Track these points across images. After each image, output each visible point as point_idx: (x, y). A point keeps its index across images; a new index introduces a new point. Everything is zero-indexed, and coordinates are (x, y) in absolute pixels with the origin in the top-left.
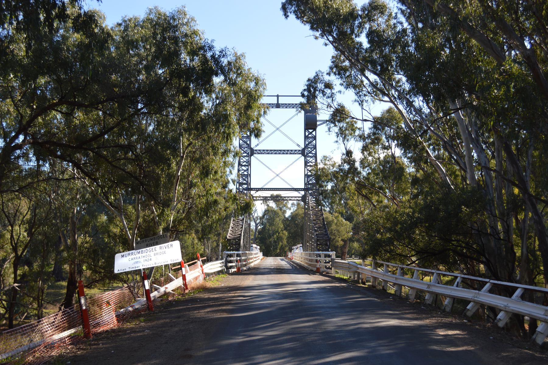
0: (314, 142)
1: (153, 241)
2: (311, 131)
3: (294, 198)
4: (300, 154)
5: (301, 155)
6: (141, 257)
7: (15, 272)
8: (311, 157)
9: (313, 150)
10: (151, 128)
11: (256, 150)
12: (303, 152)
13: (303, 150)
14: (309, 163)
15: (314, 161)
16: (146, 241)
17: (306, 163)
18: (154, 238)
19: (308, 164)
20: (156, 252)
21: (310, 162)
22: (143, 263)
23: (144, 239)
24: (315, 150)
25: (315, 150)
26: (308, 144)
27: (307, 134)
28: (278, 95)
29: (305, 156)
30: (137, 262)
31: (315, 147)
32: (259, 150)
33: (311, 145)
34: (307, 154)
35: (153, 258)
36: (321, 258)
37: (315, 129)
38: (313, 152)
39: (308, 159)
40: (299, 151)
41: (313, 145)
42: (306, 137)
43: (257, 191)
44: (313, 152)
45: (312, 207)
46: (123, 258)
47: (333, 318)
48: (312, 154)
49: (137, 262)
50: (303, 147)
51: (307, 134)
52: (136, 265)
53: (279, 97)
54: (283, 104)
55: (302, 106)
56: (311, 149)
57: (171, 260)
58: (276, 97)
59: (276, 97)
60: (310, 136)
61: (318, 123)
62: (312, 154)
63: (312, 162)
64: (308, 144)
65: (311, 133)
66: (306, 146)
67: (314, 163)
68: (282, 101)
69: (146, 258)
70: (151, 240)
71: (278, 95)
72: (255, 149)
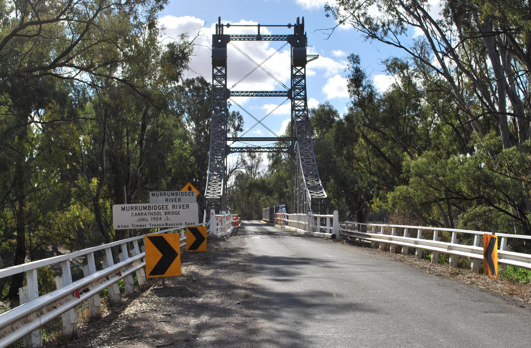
0: (303, 81)
2: (299, 68)
3: (263, 150)
4: (285, 96)
5: (287, 98)
6: (147, 214)
8: (300, 100)
9: (302, 92)
10: (108, 73)
11: (233, 92)
12: (289, 94)
14: (297, 107)
15: (303, 104)
16: (165, 194)
17: (293, 107)
18: (177, 194)
19: (296, 109)
20: (167, 211)
21: (298, 106)
22: (150, 222)
24: (304, 92)
25: (304, 92)
26: (296, 85)
27: (303, 71)
29: (293, 99)
31: (304, 88)
32: (237, 92)
33: (300, 85)
34: (295, 96)
35: (164, 217)
36: (327, 227)
37: (304, 67)
38: (302, 94)
39: (296, 102)
40: (285, 92)
41: (302, 86)
42: (293, 76)
43: (235, 141)
44: (302, 94)
47: (266, 299)
48: (301, 96)
49: (143, 220)
50: (290, 88)
51: (294, 72)
52: (142, 223)
53: (261, 28)
54: (265, 36)
55: (290, 39)
56: (300, 90)
59: (257, 27)
60: (298, 74)
61: (308, 59)
62: (301, 96)
63: (300, 106)
64: (296, 85)
65: (299, 71)
66: (293, 87)
67: (303, 108)
68: (265, 31)
69: (153, 216)
70: (173, 194)
72: (231, 90)
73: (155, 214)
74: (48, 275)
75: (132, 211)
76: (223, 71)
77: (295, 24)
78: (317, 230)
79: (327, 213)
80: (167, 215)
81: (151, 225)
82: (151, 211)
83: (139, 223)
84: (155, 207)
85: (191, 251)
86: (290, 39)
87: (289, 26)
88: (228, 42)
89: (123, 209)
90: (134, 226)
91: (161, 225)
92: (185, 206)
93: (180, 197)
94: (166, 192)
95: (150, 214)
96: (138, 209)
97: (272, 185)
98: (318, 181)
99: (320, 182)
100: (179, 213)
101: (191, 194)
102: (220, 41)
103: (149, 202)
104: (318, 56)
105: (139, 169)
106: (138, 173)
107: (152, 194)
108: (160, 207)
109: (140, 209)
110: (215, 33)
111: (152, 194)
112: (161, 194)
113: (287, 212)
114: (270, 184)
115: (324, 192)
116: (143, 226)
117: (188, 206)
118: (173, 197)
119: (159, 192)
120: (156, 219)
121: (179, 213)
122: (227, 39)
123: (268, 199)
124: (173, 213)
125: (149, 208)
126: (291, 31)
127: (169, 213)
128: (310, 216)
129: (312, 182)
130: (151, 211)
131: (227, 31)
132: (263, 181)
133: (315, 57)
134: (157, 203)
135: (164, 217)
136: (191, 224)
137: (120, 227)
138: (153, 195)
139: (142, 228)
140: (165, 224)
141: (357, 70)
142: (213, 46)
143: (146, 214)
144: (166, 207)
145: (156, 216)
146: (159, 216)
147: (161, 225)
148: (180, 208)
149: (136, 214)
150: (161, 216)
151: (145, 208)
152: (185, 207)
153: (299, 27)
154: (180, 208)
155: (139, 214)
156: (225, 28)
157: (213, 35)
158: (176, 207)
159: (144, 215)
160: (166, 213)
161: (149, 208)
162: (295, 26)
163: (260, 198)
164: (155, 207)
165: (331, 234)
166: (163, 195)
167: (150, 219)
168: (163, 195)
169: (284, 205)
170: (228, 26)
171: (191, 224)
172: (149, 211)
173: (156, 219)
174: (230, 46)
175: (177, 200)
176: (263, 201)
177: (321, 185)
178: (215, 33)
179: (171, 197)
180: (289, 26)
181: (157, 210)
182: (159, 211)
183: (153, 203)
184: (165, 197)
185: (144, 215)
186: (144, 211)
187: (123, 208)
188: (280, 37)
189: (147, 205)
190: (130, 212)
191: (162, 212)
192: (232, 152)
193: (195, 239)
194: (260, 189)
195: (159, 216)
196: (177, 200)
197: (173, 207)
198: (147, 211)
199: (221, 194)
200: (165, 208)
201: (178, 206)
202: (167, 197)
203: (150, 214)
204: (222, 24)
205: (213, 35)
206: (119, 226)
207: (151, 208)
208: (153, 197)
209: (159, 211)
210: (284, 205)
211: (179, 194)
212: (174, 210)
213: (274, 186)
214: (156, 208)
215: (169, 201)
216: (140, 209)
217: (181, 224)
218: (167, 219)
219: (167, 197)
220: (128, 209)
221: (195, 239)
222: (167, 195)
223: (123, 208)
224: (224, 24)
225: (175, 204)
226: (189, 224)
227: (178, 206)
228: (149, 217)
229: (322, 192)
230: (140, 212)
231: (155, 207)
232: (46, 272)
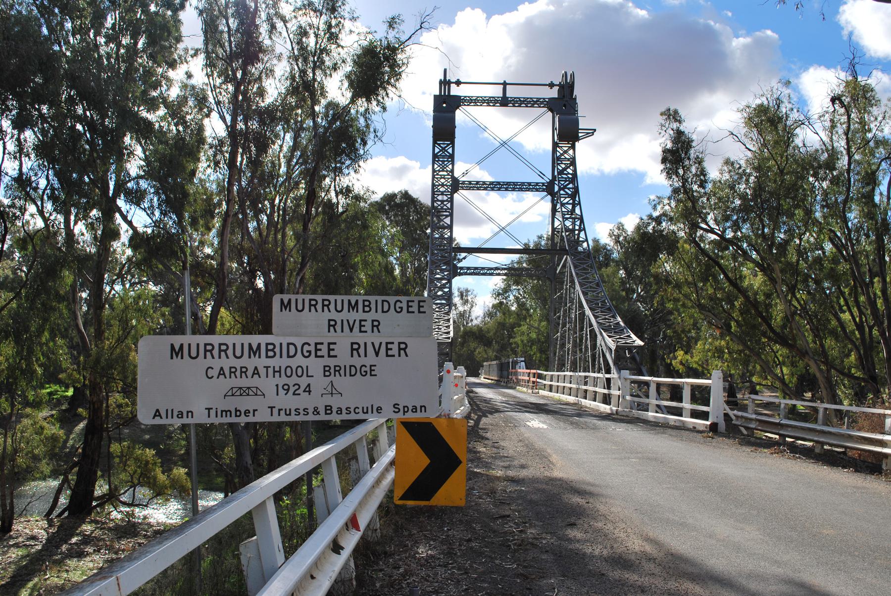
1: (360, 315)
5: (546, 193)
6: (262, 371)
7: (297, 65)
12: (549, 188)
13: (551, 184)
16: (326, 305)
20: (332, 362)
22: (272, 398)
23: (319, 298)
28: (505, 82)
30: (244, 391)
45: (560, 297)
46: (177, 360)
49: (244, 391)
52: (245, 403)
57: (395, 406)
58: (502, 86)
59: (502, 86)
68: (511, 92)
69: (284, 380)
70: (353, 307)
71: (505, 82)
73: (289, 371)
74: (151, 466)
75: (209, 361)
76: (450, 151)
77: (560, 83)
78: (650, 408)
79: (644, 370)
80: (332, 378)
81: (275, 411)
82: (275, 362)
83: (232, 404)
84: (292, 348)
85: (410, 503)
86: (551, 105)
87: (551, 85)
88: (458, 108)
89: (176, 352)
90: (213, 412)
91: (311, 411)
92: (395, 347)
93: (379, 316)
94: (332, 298)
95: (271, 371)
96: (230, 352)
97: (491, 334)
98: (614, 317)
99: (619, 319)
100: (371, 371)
101: (415, 308)
102: (444, 105)
103: (267, 330)
104: (595, 130)
105: (299, 278)
106: (297, 286)
107: (282, 300)
108: (306, 348)
109: (238, 354)
110: (438, 93)
111: (282, 300)
112: (313, 305)
113: (527, 368)
114: (489, 332)
115: (633, 335)
116: (247, 412)
117: (403, 348)
118: (354, 316)
119: (307, 297)
120: (292, 390)
121: (371, 371)
122: (457, 102)
123: (485, 351)
124: (352, 371)
125: (271, 350)
126: (554, 93)
127: (337, 370)
128: (626, 379)
129: (605, 319)
130: (275, 362)
131: (455, 91)
132: (480, 329)
133: (588, 133)
134: (297, 335)
135: (319, 382)
136: (415, 410)
137: (163, 415)
138: (285, 306)
139: (243, 420)
140: (322, 410)
141: (679, 133)
142: (434, 111)
143: (256, 372)
144: (329, 350)
145: (294, 379)
146: (304, 382)
147: (311, 411)
148: (377, 354)
149: (222, 372)
150: (309, 380)
151: (254, 351)
152: (395, 351)
153: (567, 89)
154: (377, 354)
155: (233, 371)
156: (453, 86)
157: (435, 96)
158: (362, 351)
159: (250, 373)
160: (326, 370)
161: (271, 350)
162: (560, 85)
163: (475, 349)
164: (290, 351)
165: (708, 423)
166: (319, 307)
167: (270, 390)
168: (319, 307)
169: (523, 359)
170: (458, 83)
171: (415, 410)
172: (270, 362)
173: (292, 390)
174: (460, 115)
175: (368, 326)
176: (479, 353)
177: (622, 324)
178: (438, 93)
179: (345, 315)
180: (551, 85)
181: (299, 360)
182: (304, 362)
183: (284, 335)
184: (327, 315)
185: (250, 373)
186: (251, 363)
187: (177, 348)
188: (490, 185)
189: (263, 339)
190: (202, 363)
191: (315, 365)
192: (460, 274)
193: (425, 461)
194: (477, 338)
195: (304, 382)
196: (368, 326)
197: (355, 348)
198: (261, 362)
199: (452, 334)
200: (324, 351)
201: (370, 349)
202: (334, 315)
203: (271, 371)
204: (449, 80)
205: (435, 96)
206: (157, 414)
207: (277, 350)
208: (286, 312)
209: (304, 362)
210: (523, 359)
211: (373, 306)
212: (357, 361)
213: (495, 334)
214: (292, 353)
215: (338, 328)
216: (238, 354)
217: (379, 409)
218: (333, 391)
219: (334, 315)
220: (194, 354)
221: (425, 461)
222: (332, 307)
223: (177, 348)
224: (452, 81)
225: (360, 338)
226: (406, 410)
227: (370, 349)
228: (267, 384)
229: (629, 336)
230: (238, 364)
231: (292, 348)
232: (147, 462)
